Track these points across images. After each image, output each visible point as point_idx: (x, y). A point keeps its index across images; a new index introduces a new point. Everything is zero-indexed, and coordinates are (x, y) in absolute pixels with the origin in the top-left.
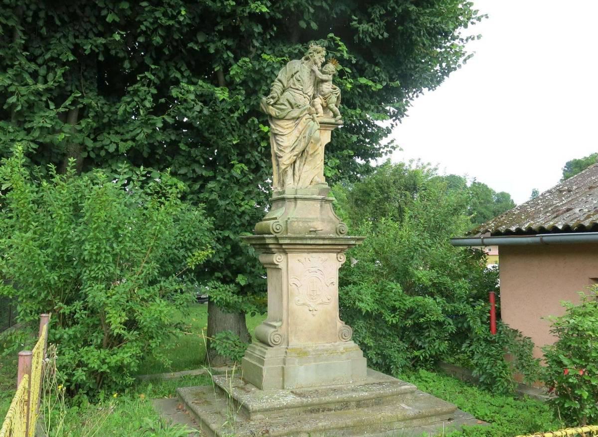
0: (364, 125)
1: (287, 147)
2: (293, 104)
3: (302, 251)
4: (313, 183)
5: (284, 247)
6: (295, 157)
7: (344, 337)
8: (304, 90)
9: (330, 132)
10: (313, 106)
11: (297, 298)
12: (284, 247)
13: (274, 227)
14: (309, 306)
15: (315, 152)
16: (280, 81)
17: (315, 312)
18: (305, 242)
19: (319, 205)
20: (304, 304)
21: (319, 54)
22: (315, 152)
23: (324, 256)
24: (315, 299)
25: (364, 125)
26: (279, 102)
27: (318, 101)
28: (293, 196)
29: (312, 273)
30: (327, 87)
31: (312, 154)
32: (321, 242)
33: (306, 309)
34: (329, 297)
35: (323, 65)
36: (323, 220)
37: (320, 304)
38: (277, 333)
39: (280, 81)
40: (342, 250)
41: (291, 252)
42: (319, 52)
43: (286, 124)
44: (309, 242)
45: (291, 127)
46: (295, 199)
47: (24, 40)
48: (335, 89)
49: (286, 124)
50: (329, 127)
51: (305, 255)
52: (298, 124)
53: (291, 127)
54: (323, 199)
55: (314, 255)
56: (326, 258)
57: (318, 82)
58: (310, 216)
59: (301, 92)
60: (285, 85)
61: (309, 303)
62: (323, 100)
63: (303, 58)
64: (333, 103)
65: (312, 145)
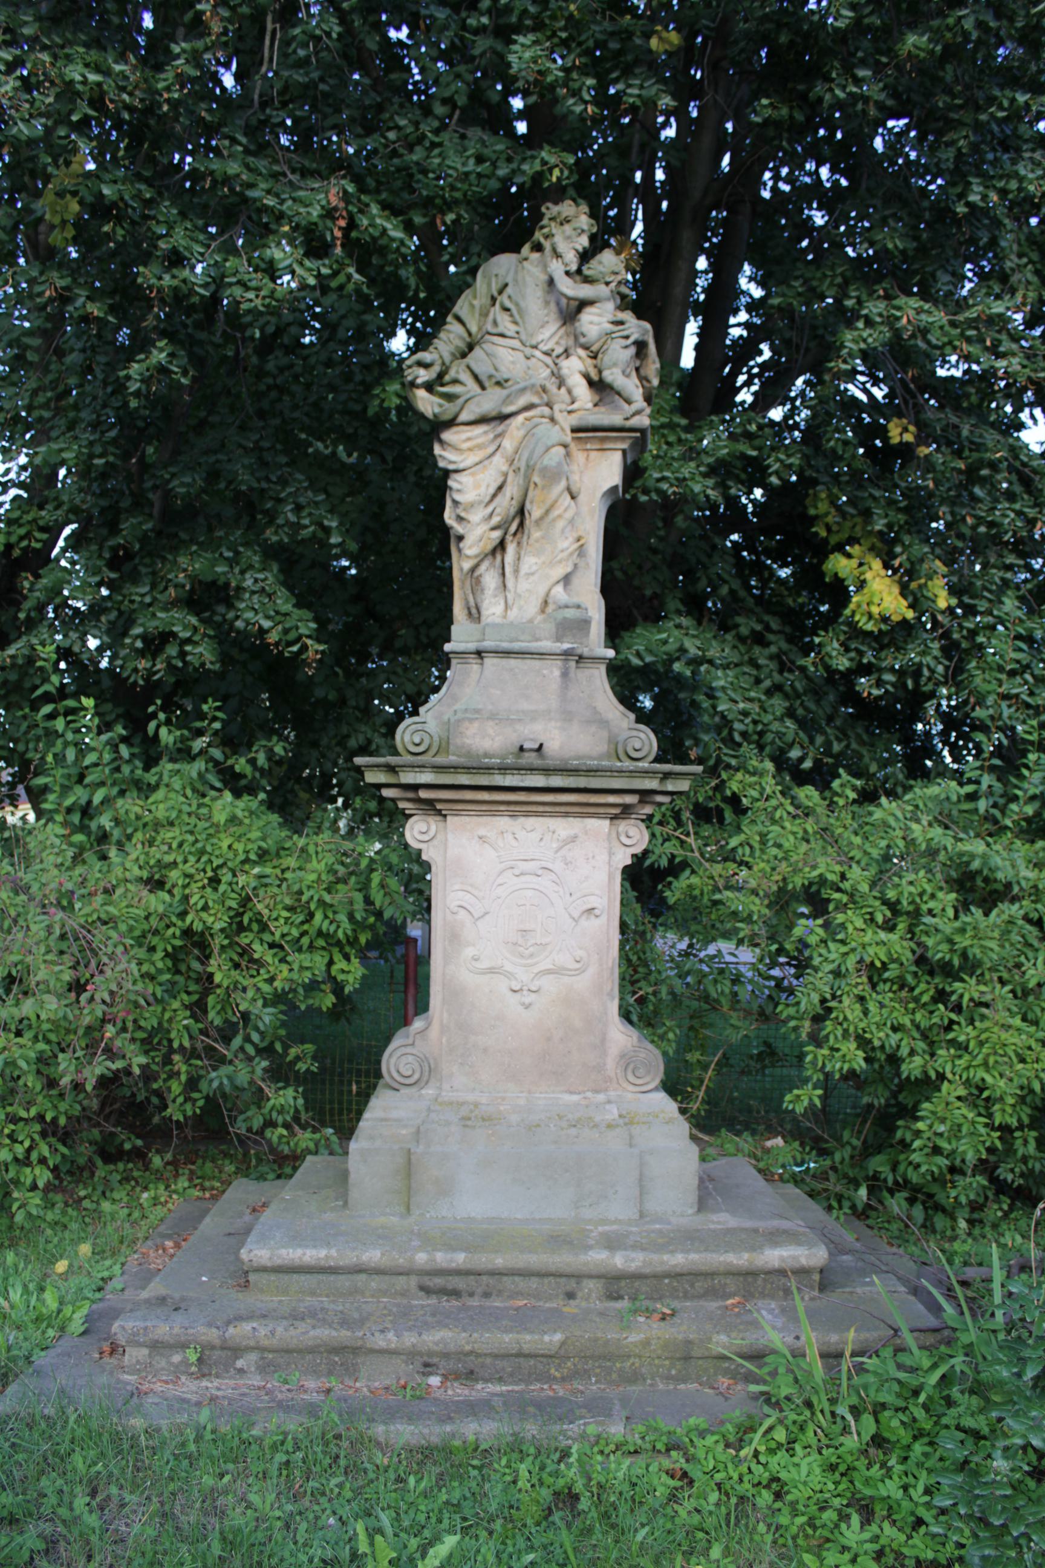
0: (875, 422)
1: (472, 505)
2: (483, 378)
3: (491, 809)
4: (550, 608)
5: (423, 794)
6: (497, 534)
7: (631, 1078)
8: (523, 337)
9: (618, 456)
10: (561, 383)
11: (469, 952)
12: (423, 794)
13: (407, 738)
14: (509, 975)
15: (547, 512)
16: (458, 319)
17: (529, 998)
18: (484, 780)
19: (557, 673)
20: (491, 971)
21: (567, 228)
22: (547, 512)
23: (564, 827)
24: (531, 956)
25: (875, 422)
26: (447, 378)
27: (574, 367)
28: (472, 646)
29: (523, 878)
30: (595, 322)
31: (542, 518)
32: (539, 781)
33: (502, 985)
34: (580, 953)
35: (585, 256)
36: (567, 716)
37: (549, 972)
38: (409, 1050)
39: (458, 319)
40: (626, 811)
41: (457, 813)
42: (567, 221)
43: (464, 436)
44: (499, 780)
45: (480, 447)
46: (479, 654)
47: (231, 285)
48: (622, 323)
49: (464, 436)
50: (616, 439)
51: (503, 822)
52: (500, 435)
53: (480, 447)
54: (567, 654)
55: (532, 822)
56: (572, 832)
57: (572, 312)
58: (525, 706)
59: (516, 343)
60: (474, 329)
61: (508, 967)
62: (589, 361)
63: (526, 250)
64: (615, 365)
65: (538, 492)
